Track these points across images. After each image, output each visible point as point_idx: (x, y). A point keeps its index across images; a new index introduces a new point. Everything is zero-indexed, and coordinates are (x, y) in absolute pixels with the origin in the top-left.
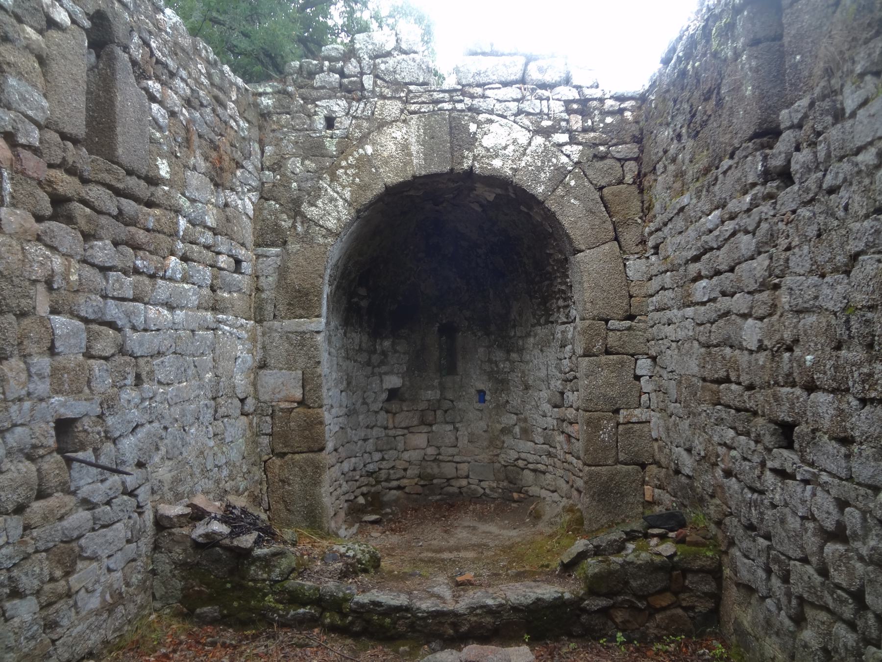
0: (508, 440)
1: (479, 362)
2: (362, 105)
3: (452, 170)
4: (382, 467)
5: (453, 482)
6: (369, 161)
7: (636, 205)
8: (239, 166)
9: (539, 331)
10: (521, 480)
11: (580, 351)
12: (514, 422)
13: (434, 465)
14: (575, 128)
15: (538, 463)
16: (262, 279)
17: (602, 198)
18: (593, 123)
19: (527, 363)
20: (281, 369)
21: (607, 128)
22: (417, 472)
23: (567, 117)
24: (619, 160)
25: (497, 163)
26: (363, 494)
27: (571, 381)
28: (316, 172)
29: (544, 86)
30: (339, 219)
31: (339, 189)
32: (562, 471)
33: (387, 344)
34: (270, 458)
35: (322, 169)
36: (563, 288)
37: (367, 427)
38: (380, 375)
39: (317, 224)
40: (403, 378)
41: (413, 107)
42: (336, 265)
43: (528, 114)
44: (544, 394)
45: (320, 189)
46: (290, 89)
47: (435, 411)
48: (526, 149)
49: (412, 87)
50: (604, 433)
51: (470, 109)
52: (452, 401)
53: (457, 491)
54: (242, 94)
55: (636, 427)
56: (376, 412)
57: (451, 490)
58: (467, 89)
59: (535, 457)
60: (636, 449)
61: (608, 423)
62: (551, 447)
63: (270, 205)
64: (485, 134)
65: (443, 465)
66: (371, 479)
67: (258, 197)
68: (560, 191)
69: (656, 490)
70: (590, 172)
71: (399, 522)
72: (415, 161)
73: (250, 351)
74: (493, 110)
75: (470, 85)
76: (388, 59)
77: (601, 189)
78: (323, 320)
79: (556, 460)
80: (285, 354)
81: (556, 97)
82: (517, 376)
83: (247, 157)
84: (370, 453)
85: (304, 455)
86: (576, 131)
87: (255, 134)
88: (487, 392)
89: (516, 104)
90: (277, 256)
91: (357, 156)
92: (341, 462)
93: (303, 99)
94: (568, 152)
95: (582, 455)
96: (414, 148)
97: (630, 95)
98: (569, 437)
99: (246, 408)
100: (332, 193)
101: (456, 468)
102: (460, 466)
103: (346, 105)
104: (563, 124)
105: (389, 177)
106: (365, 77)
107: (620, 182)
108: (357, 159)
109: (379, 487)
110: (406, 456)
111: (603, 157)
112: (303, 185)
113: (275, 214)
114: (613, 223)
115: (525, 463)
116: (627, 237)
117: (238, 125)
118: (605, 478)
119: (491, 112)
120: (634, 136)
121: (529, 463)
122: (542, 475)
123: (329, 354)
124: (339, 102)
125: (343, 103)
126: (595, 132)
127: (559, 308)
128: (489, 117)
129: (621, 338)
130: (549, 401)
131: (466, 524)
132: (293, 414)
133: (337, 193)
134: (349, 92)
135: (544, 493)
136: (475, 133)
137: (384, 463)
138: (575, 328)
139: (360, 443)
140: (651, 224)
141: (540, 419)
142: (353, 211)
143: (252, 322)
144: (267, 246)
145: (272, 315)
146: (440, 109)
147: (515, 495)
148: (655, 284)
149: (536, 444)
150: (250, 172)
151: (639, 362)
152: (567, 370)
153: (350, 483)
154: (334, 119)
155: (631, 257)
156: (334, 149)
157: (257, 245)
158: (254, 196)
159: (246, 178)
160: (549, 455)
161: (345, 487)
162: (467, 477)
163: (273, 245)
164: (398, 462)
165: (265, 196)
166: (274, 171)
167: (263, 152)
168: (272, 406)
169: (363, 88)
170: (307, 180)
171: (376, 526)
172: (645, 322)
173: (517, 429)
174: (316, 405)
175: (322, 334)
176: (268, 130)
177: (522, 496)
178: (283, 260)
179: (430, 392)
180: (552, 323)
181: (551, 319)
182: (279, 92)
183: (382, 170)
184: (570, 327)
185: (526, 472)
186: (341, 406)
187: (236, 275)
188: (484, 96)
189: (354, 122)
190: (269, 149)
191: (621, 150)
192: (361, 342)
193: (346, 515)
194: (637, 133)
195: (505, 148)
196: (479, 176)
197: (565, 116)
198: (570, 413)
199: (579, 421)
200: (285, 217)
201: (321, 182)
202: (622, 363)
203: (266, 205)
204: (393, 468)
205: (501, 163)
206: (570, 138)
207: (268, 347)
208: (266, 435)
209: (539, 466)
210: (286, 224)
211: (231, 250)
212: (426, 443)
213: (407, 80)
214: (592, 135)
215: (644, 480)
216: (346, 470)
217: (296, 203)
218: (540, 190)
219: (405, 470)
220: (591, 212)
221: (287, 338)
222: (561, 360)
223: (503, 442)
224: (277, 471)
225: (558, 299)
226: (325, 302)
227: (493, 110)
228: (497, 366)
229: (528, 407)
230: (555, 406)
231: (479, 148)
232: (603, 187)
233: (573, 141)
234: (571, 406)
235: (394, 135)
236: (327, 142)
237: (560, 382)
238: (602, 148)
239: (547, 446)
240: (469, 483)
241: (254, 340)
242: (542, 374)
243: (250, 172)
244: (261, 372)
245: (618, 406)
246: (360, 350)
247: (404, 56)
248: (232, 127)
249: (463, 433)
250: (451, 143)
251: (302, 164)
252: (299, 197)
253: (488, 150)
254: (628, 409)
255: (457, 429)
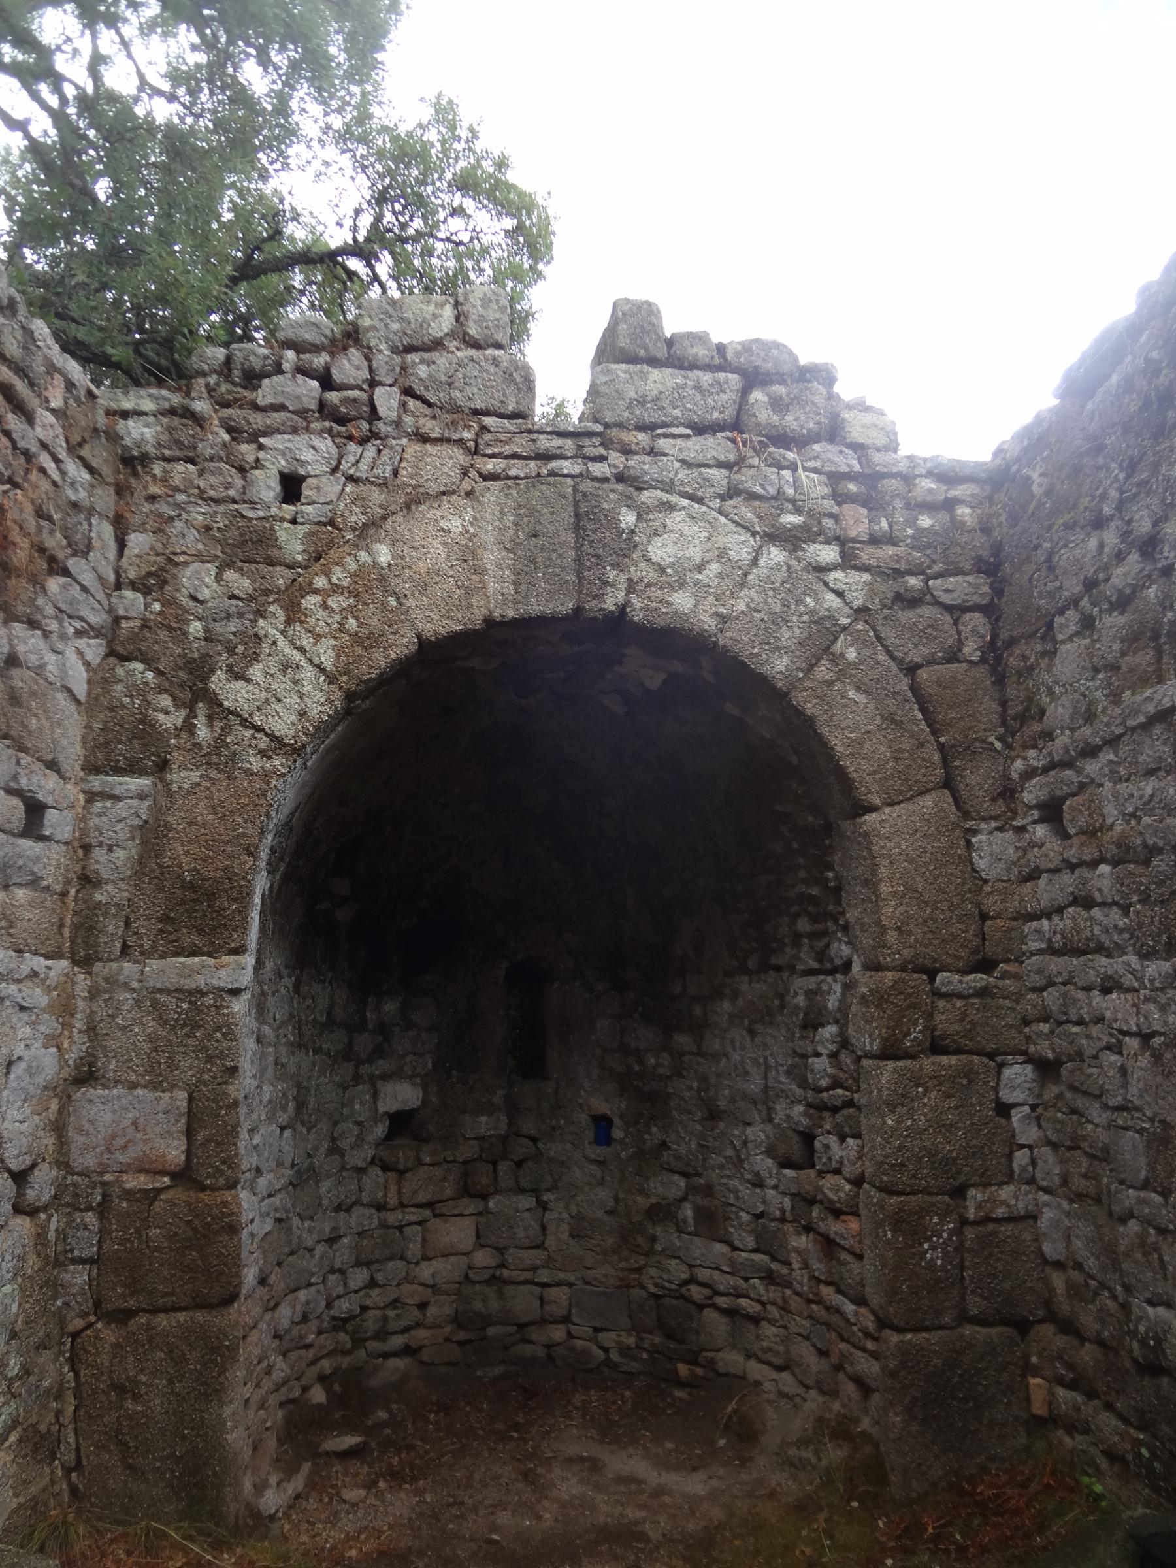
0: (666, 1236)
1: (598, 1051)
2: (370, 451)
3: (578, 610)
4: (368, 1302)
5: (534, 1334)
6: (382, 579)
7: (989, 707)
8: (57, 568)
9: (745, 987)
10: (698, 1334)
11: (868, 1042)
12: (680, 1194)
13: (491, 1292)
14: (853, 533)
15: (739, 1296)
16: (99, 854)
17: (914, 688)
18: (890, 526)
19: (715, 1057)
20: (133, 1086)
21: (921, 541)
22: (448, 1310)
23: (835, 509)
24: (949, 608)
25: (682, 600)
26: (322, 1379)
27: (835, 1110)
28: (251, 598)
29: (782, 439)
30: (302, 714)
31: (306, 641)
32: (807, 1324)
33: (390, 1007)
34: (90, 1325)
35: (267, 592)
36: (815, 891)
37: (338, 1208)
38: (373, 1080)
39: (246, 723)
40: (425, 1087)
41: (490, 466)
42: (287, 824)
43: (752, 496)
44: (758, 1133)
45: (258, 639)
46: (201, 406)
47: (494, 1163)
48: (746, 574)
49: (489, 421)
50: (933, 1248)
51: (620, 478)
52: (534, 1140)
53: (541, 1352)
54: (77, 400)
55: (1006, 1230)
56: (361, 1171)
57: (526, 1350)
58: (614, 433)
59: (732, 1280)
60: (1007, 1285)
61: (942, 1222)
62: (774, 1259)
63: (131, 673)
64: (656, 534)
65: (509, 1290)
66: (342, 1336)
67: (102, 651)
68: (823, 671)
69: (1061, 1392)
70: (887, 632)
71: (410, 1447)
72: (492, 586)
73: (52, 1040)
74: (672, 481)
75: (620, 425)
76: (434, 355)
77: (911, 670)
78: (249, 960)
79: (788, 1292)
80: (146, 1047)
81: (811, 464)
82: (690, 1088)
83: (84, 550)
84: (342, 1272)
85: (181, 1316)
86: (854, 540)
87: (105, 499)
88: (617, 1121)
89: (725, 473)
90: (142, 797)
91: (353, 566)
92: (273, 1309)
93: (229, 430)
94: (839, 586)
95: (875, 1300)
96: (491, 557)
97: (967, 472)
98: (829, 1245)
99: (31, 1194)
100: (287, 650)
101: (541, 1299)
102: (553, 1293)
103: (334, 450)
104: (828, 523)
105: (430, 620)
106: (378, 391)
107: (953, 656)
108: (353, 575)
109: (361, 1354)
110: (425, 1272)
111: (910, 601)
112: (218, 627)
113: (142, 695)
114: (941, 747)
115: (707, 1292)
116: (972, 779)
117: (63, 473)
118: (937, 1361)
119: (668, 486)
120: (979, 560)
121: (717, 1293)
122: (752, 1327)
123: (259, 1040)
124: (317, 442)
125: (326, 445)
126: (895, 544)
127: (797, 937)
128: (666, 497)
129: (965, 1015)
130: (770, 1152)
131: (573, 1449)
132: (157, 1206)
133: (302, 650)
134: (342, 420)
135: (755, 1370)
136: (633, 531)
137: (375, 1293)
138: (847, 987)
139: (320, 1249)
140: (1032, 753)
141: (745, 1191)
142: (338, 695)
143: (64, 963)
144: (118, 771)
145: (118, 945)
146: (552, 474)
147: (683, 1369)
148: (1047, 891)
149: (735, 1249)
150: (85, 589)
151: (1007, 1072)
152: (824, 1083)
153: (292, 1356)
154: (303, 479)
155: (983, 826)
156: (300, 548)
157: (92, 768)
158: (94, 649)
159: (73, 602)
160: (770, 1278)
161: (281, 1368)
162: (566, 1319)
163: (132, 769)
164: (406, 1288)
165: (120, 649)
166: (146, 591)
167: (122, 545)
168: (104, 1184)
169: (374, 415)
170: (228, 617)
171: (354, 1465)
172: (1016, 977)
173: (687, 1212)
174: (222, 1181)
175: (247, 996)
176: (139, 494)
177: (699, 1371)
178: (156, 809)
179: (484, 1119)
180: (778, 969)
181: (774, 961)
182: (172, 412)
183: (411, 602)
184: (834, 987)
185: (710, 1314)
186: (279, 1164)
187: (25, 843)
188: (652, 452)
189: (348, 489)
190: (138, 542)
191: (954, 588)
192: (332, 1004)
193: (281, 1442)
194: (985, 554)
195: (700, 568)
196: (640, 628)
197: (830, 505)
198: (835, 1188)
199: (863, 1211)
200: (166, 701)
201: (261, 622)
202: (969, 1074)
203: (120, 671)
204: (395, 1303)
205: (692, 601)
206: (843, 554)
207: (103, 1028)
208: (82, 1261)
209: (743, 1302)
210: (169, 718)
211: (15, 778)
212: (471, 1239)
213: (479, 405)
214: (891, 550)
215: (1027, 1363)
216: (285, 1323)
217: (200, 669)
218: (779, 665)
219: (423, 1306)
220: (894, 721)
221: (155, 1004)
222: (804, 1057)
223: (654, 1239)
224: (105, 1360)
225: (796, 917)
226: (255, 915)
227: (672, 481)
228: (641, 1062)
229: (715, 1160)
230: (786, 1164)
231: (642, 565)
232: (919, 666)
233: (848, 561)
234: (838, 1172)
235: (444, 524)
236: (283, 532)
237: (800, 1109)
238: (914, 582)
239: (766, 1258)
240: (570, 1335)
241: (64, 1009)
242: (754, 1085)
243: (85, 589)
244: (79, 1094)
245: (962, 1178)
246: (330, 1023)
247: (472, 352)
248: (43, 471)
249: (558, 1213)
250: (578, 549)
251: (219, 578)
252: (205, 657)
253: (662, 570)
254: (985, 1185)
255: (544, 1206)
